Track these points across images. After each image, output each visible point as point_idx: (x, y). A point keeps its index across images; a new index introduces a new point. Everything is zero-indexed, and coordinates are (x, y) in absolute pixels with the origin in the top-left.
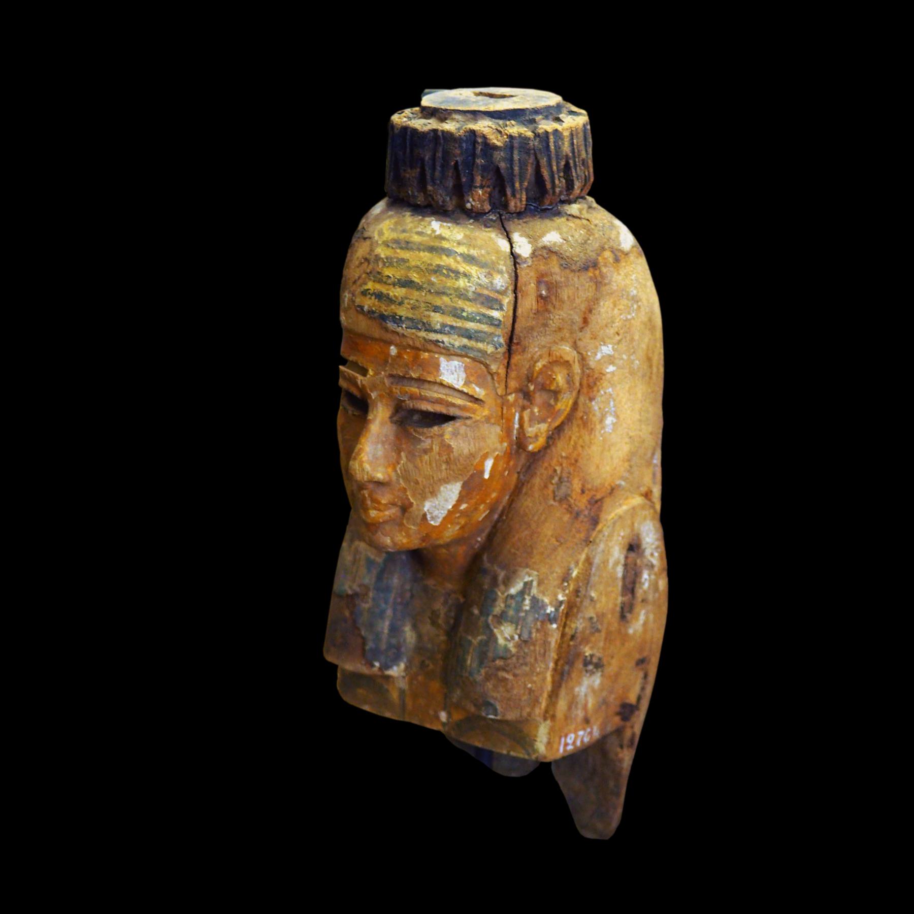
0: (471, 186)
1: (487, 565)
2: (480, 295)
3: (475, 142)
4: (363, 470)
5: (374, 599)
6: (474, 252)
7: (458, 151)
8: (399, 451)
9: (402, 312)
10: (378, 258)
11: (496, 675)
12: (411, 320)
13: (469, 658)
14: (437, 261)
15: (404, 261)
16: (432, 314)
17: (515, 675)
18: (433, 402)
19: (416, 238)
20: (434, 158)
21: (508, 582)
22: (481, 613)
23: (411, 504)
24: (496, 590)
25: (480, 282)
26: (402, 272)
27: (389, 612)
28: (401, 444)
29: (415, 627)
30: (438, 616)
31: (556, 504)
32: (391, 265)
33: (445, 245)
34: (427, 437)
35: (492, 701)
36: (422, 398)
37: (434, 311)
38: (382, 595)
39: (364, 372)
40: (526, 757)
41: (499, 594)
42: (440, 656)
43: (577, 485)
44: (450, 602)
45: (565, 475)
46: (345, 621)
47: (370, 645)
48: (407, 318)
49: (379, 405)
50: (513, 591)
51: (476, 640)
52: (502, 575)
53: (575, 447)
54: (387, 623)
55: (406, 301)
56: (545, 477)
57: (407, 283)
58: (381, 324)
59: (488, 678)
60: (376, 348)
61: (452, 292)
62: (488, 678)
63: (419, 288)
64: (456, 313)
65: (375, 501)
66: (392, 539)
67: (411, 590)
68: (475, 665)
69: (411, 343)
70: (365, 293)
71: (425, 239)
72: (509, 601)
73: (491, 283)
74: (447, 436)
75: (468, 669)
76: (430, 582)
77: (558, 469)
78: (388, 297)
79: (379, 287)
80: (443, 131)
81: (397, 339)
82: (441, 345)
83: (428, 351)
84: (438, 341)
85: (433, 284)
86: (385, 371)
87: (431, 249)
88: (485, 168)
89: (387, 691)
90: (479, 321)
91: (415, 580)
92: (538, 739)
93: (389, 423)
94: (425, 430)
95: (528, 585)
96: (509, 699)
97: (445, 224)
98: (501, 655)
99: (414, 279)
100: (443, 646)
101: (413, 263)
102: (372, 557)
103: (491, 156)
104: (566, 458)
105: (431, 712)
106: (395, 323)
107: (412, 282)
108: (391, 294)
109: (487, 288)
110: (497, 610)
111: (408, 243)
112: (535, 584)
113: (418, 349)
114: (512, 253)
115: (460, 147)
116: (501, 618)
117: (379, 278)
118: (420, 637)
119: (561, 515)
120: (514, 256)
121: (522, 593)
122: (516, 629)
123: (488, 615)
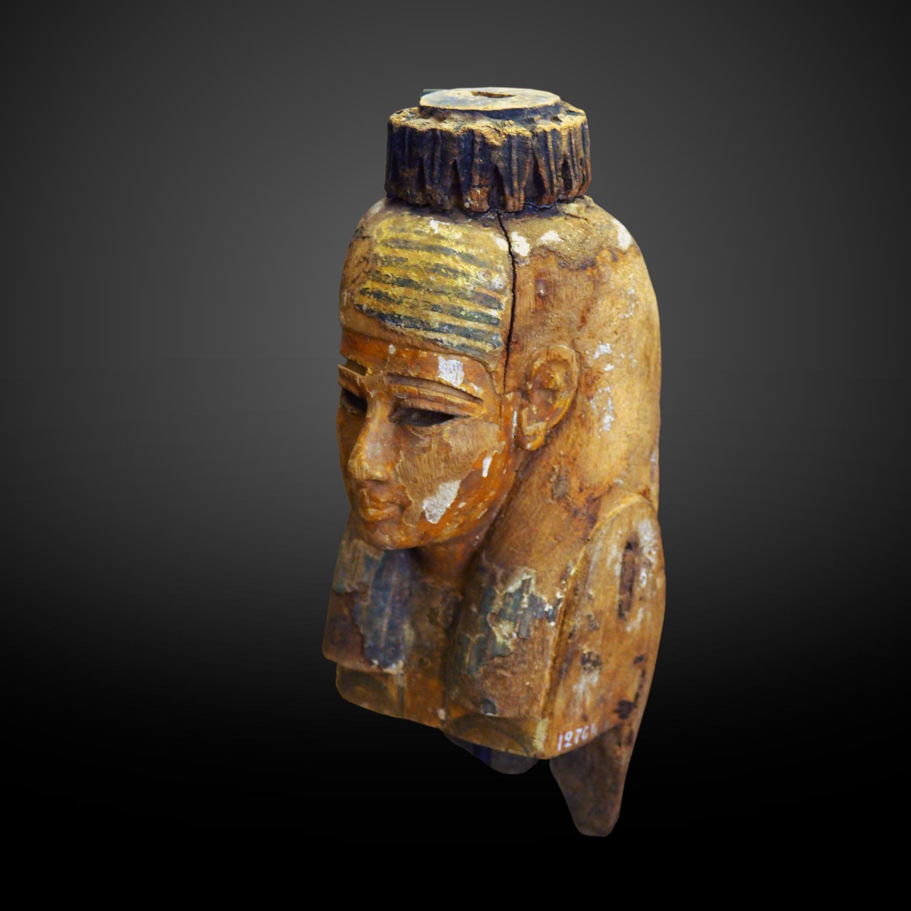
0: (470, 185)
1: (485, 563)
2: (478, 294)
3: (473, 142)
4: (362, 468)
5: (372, 597)
6: (472, 251)
7: (456, 151)
8: (397, 450)
9: (401, 311)
10: (376, 257)
11: (494, 673)
12: (410, 319)
13: (468, 656)
14: (435, 260)
15: (402, 260)
16: (431, 313)
17: (513, 673)
18: (432, 401)
19: (415, 238)
20: (432, 158)
21: (506, 580)
22: (480, 611)
23: (410, 503)
24: (495, 588)
25: (478, 281)
26: (401, 271)
27: (388, 610)
28: (400, 443)
29: (413, 625)
30: (437, 614)
31: (554, 502)
32: (390, 264)
33: (444, 244)
34: (425, 436)
35: (490, 699)
36: (421, 397)
37: (433, 310)
38: (380, 593)
39: (363, 371)
40: (525, 754)
41: (498, 592)
42: (439, 654)
43: (575, 483)
44: (449, 600)
45: (563, 473)
46: (344, 619)
47: (369, 643)
48: (406, 317)
50: (511, 589)
51: (474, 638)
52: (500, 573)
53: (573, 446)
54: (386, 621)
55: (405, 300)
56: (543, 475)
57: (406, 282)
58: (380, 323)
59: (486, 675)
60: (375, 347)
61: (450, 291)
62: (486, 675)
63: (418, 287)
64: (455, 312)
65: (374, 499)
66: (391, 537)
67: (410, 588)
68: (473, 663)
69: (410, 342)
70: (363, 292)
71: (423, 238)
72: (508, 599)
73: (490, 282)
74: (445, 435)
75: (467, 667)
76: (429, 580)
77: (556, 467)
78: (386, 296)
79: (378, 286)
80: (441, 131)
81: (396, 338)
82: (440, 344)
83: (427, 350)
84: (436, 340)
85: (431, 283)
86: (384, 370)
87: (430, 248)
88: (483, 168)
89: (386, 688)
90: (478, 320)
91: (414, 578)
92: (537, 737)
93: (388, 422)
94: (424, 428)
95: (526, 584)
96: (507, 697)
97: (443, 223)
98: (500, 653)
99: (413, 278)
100: (442, 644)
101: (412, 263)
102: (371, 555)
103: (490, 155)
104: (565, 456)
105: (430, 710)
106: (394, 322)
107: (411, 281)
108: (390, 293)
109: (485, 287)
110: (495, 608)
111: (406, 242)
112: (533, 582)
113: (417, 348)
114: (510, 252)
115: (459, 146)
116: (500, 616)
117: (378, 277)
118: (418, 635)
119: (559, 514)
120: (513, 256)
121: (520, 591)
122: (515, 627)
123: (486, 613)
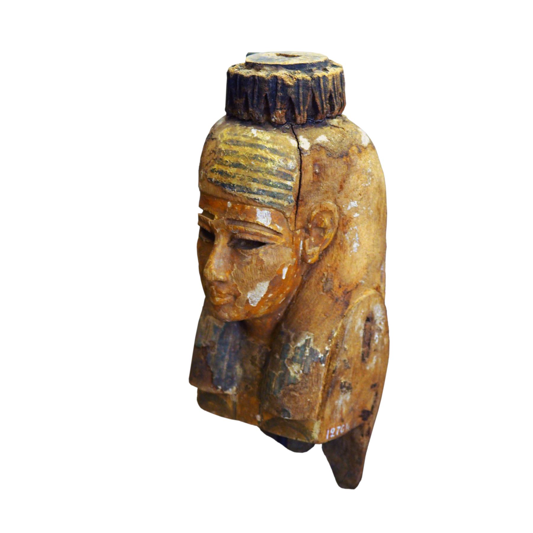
0: (275, 108)
1: (284, 329)
2: (280, 172)
3: (277, 83)
4: (212, 274)
5: (218, 349)
6: (276, 147)
7: (267, 88)
8: (232, 263)
9: (235, 182)
10: (220, 150)
11: (289, 394)
12: (240, 186)
13: (274, 384)
14: (255, 152)
15: (235, 152)
16: (252, 183)
17: (300, 394)
18: (253, 235)
19: (243, 139)
20: (253, 92)
21: (296, 339)
22: (281, 357)
23: (240, 294)
24: (289, 344)
25: (280, 164)
26: (235, 159)
27: (227, 357)
28: (234, 259)
29: (242, 366)
30: (255, 360)
31: (324, 294)
32: (228, 154)
33: (260, 143)
34: (249, 255)
35: (287, 409)
36: (246, 232)
37: (253, 181)
38: (223, 347)
40: (307, 441)
41: (291, 346)
42: (257, 382)
43: (336, 283)
44: (262, 351)
45: (329, 277)
46: (201, 362)
47: (216, 376)
48: (237, 185)
49: (221, 236)
50: (299, 345)
51: (278, 374)
52: (293, 335)
53: (335, 261)
54: (226, 363)
55: (237, 176)
56: (318, 278)
57: (237, 165)
58: (222, 189)
59: (284, 395)
60: (219, 203)
61: (263, 170)
62: (284, 395)
63: (244, 168)
64: (266, 183)
65: (219, 292)
66: (229, 314)
67: (240, 344)
68: (277, 388)
69: (240, 200)
70: (213, 171)
71: (248, 139)
72: (297, 351)
73: (287, 165)
74: (261, 254)
75: (273, 390)
76: (251, 340)
77: (326, 273)
78: (226, 173)
79: (221, 168)
80: (258, 77)
81: (232, 198)
82: (257, 201)
83: (250, 205)
84: (255, 199)
85: (252, 166)
86: (225, 216)
87: (252, 145)
88: (283, 98)
89: (226, 403)
90: (280, 187)
91: (242, 338)
92: (314, 431)
93: (227, 247)
94: (248, 251)
95: (308, 341)
96: (297, 408)
97: (259, 131)
98: (292, 382)
99: (241, 163)
100: (258, 377)
101: (241, 154)
102: (217, 325)
103: (287, 91)
104: (330, 267)
105: (252, 415)
106: (230, 188)
107: (240, 164)
108: (228, 171)
109: (284, 168)
110: (290, 356)
111: (238, 141)
112: (312, 340)
113: (244, 204)
114: (298, 148)
115: (269, 86)
116: (292, 360)
117: (221, 162)
118: (245, 371)
119: (327, 301)
120: (300, 150)
121: (304, 346)
122: (301, 367)
123: (285, 359)
